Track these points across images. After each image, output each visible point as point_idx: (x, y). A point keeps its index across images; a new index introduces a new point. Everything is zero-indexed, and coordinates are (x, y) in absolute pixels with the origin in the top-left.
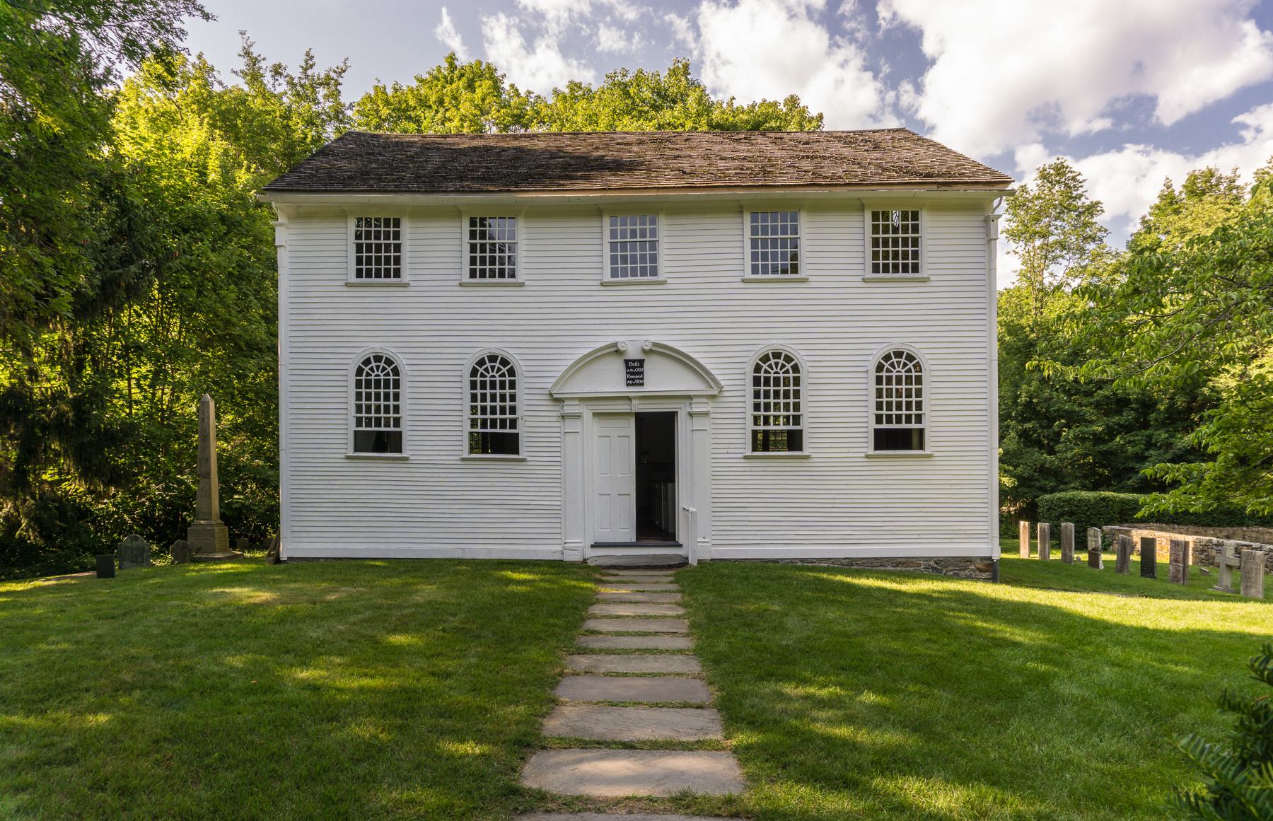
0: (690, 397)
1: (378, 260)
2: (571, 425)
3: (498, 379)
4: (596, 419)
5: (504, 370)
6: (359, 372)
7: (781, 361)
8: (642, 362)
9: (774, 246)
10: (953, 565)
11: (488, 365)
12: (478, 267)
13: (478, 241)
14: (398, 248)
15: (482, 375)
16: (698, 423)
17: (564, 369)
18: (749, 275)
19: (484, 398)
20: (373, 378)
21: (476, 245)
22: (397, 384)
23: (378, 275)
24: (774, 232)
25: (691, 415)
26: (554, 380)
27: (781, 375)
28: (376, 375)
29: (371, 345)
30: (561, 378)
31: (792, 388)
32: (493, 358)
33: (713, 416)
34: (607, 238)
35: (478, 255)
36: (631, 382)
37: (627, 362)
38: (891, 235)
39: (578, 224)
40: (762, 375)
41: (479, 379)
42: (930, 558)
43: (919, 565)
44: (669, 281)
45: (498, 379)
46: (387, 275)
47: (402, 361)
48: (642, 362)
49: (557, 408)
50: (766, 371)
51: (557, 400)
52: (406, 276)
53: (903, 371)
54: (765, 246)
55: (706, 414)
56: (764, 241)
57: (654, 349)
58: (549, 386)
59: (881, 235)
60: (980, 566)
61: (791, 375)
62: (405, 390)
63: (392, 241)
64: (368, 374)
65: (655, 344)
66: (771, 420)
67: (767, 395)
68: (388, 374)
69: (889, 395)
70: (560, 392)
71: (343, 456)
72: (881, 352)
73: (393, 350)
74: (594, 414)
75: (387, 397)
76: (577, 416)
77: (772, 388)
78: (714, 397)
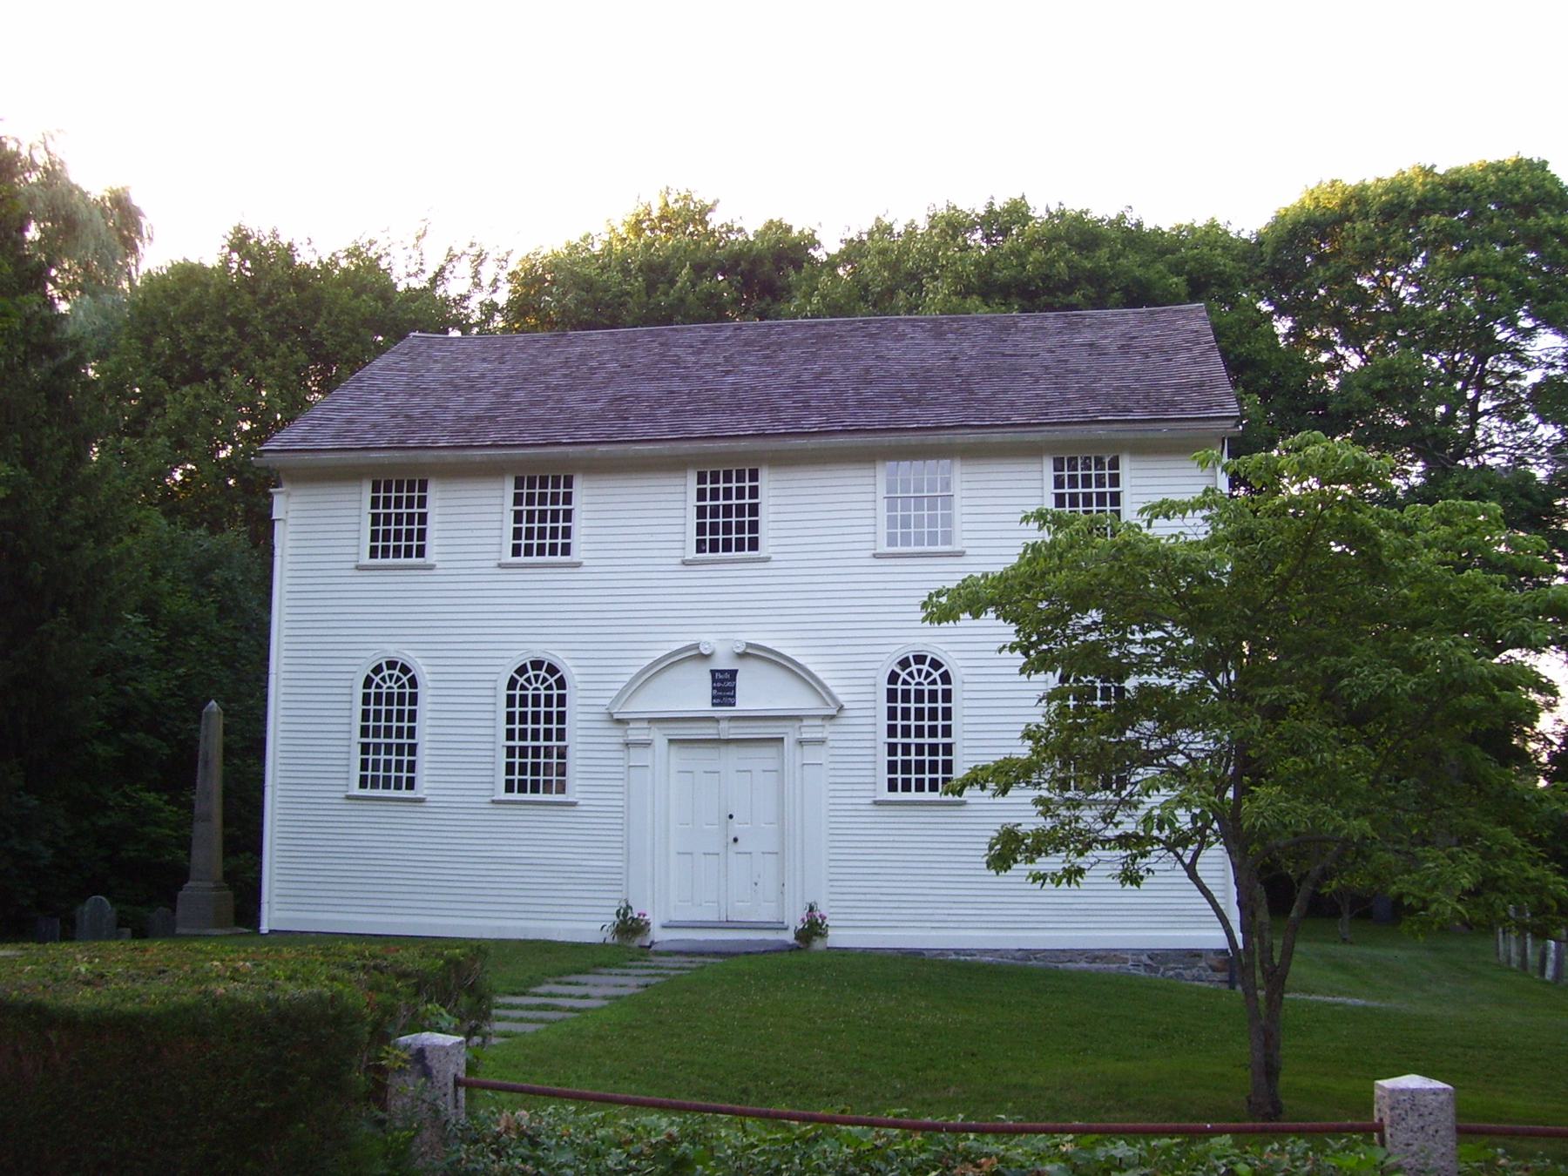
0: (799, 718)
1: (727, 527)
2: (637, 756)
3: (543, 693)
4: (674, 748)
5: (552, 680)
6: (368, 682)
7: (925, 667)
8: (734, 673)
9: (399, 522)
10: (1174, 961)
11: (531, 673)
12: (523, 542)
13: (524, 507)
14: (423, 518)
15: (523, 688)
16: (811, 755)
17: (627, 678)
18: (366, 559)
19: (906, 715)
20: (384, 690)
21: (521, 511)
22: (414, 699)
23: (727, 548)
24: (542, 501)
25: (801, 742)
26: (614, 694)
27: (926, 688)
28: (389, 688)
29: (386, 646)
30: (622, 692)
31: (940, 705)
32: (537, 665)
33: (831, 744)
34: (882, 491)
35: (524, 525)
36: (718, 701)
37: (713, 672)
38: (734, 501)
39: (1001, 468)
40: (899, 687)
41: (518, 692)
42: (1142, 951)
43: (1125, 961)
44: (774, 557)
45: (543, 693)
46: (740, 548)
47: (422, 670)
48: (734, 673)
49: (619, 733)
50: (905, 682)
51: (619, 721)
52: (432, 555)
53: (542, 687)
54: (530, 519)
55: (822, 742)
56: (388, 517)
57: (749, 651)
58: (607, 702)
59: (708, 503)
60: (1214, 963)
61: (939, 687)
62: (424, 708)
63: (392, 510)
64: (523, 688)
65: (749, 645)
66: (913, 749)
67: (906, 714)
68: (934, 682)
69: (933, 712)
70: (621, 711)
71: (343, 795)
72: (897, 655)
73: (411, 654)
74: (671, 741)
75: (906, 712)
76: (647, 744)
77: (913, 705)
78: (832, 717)
